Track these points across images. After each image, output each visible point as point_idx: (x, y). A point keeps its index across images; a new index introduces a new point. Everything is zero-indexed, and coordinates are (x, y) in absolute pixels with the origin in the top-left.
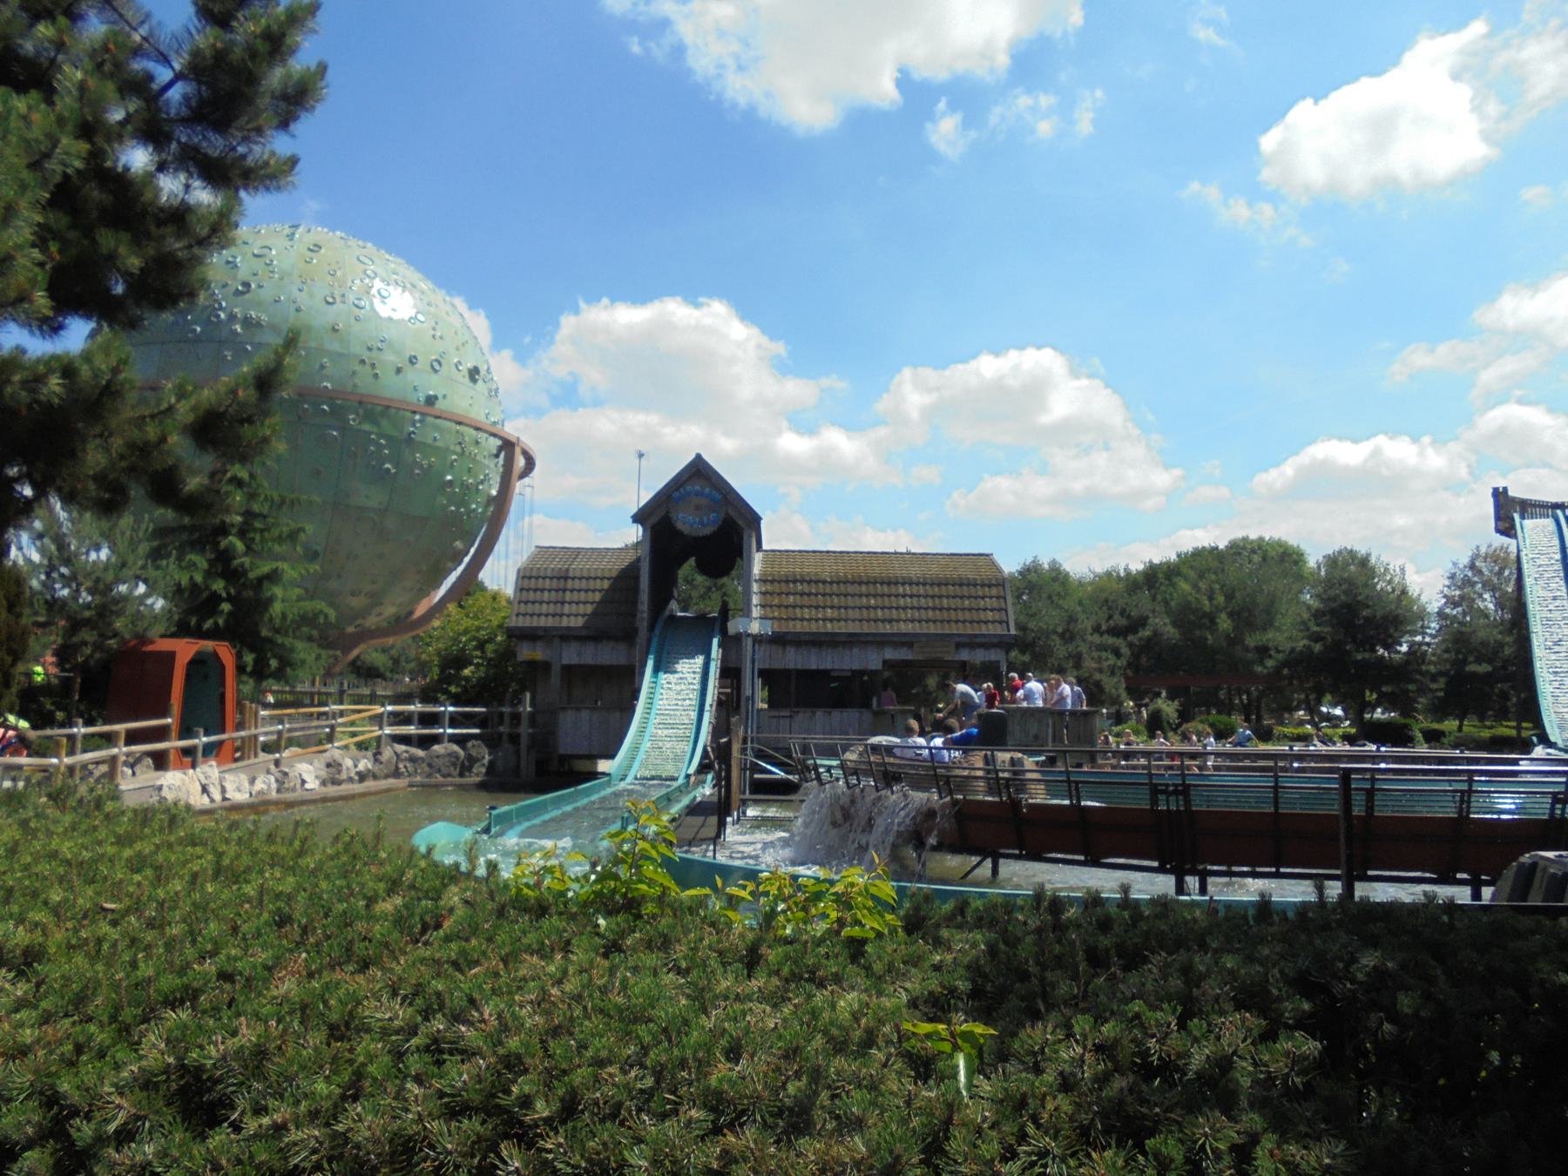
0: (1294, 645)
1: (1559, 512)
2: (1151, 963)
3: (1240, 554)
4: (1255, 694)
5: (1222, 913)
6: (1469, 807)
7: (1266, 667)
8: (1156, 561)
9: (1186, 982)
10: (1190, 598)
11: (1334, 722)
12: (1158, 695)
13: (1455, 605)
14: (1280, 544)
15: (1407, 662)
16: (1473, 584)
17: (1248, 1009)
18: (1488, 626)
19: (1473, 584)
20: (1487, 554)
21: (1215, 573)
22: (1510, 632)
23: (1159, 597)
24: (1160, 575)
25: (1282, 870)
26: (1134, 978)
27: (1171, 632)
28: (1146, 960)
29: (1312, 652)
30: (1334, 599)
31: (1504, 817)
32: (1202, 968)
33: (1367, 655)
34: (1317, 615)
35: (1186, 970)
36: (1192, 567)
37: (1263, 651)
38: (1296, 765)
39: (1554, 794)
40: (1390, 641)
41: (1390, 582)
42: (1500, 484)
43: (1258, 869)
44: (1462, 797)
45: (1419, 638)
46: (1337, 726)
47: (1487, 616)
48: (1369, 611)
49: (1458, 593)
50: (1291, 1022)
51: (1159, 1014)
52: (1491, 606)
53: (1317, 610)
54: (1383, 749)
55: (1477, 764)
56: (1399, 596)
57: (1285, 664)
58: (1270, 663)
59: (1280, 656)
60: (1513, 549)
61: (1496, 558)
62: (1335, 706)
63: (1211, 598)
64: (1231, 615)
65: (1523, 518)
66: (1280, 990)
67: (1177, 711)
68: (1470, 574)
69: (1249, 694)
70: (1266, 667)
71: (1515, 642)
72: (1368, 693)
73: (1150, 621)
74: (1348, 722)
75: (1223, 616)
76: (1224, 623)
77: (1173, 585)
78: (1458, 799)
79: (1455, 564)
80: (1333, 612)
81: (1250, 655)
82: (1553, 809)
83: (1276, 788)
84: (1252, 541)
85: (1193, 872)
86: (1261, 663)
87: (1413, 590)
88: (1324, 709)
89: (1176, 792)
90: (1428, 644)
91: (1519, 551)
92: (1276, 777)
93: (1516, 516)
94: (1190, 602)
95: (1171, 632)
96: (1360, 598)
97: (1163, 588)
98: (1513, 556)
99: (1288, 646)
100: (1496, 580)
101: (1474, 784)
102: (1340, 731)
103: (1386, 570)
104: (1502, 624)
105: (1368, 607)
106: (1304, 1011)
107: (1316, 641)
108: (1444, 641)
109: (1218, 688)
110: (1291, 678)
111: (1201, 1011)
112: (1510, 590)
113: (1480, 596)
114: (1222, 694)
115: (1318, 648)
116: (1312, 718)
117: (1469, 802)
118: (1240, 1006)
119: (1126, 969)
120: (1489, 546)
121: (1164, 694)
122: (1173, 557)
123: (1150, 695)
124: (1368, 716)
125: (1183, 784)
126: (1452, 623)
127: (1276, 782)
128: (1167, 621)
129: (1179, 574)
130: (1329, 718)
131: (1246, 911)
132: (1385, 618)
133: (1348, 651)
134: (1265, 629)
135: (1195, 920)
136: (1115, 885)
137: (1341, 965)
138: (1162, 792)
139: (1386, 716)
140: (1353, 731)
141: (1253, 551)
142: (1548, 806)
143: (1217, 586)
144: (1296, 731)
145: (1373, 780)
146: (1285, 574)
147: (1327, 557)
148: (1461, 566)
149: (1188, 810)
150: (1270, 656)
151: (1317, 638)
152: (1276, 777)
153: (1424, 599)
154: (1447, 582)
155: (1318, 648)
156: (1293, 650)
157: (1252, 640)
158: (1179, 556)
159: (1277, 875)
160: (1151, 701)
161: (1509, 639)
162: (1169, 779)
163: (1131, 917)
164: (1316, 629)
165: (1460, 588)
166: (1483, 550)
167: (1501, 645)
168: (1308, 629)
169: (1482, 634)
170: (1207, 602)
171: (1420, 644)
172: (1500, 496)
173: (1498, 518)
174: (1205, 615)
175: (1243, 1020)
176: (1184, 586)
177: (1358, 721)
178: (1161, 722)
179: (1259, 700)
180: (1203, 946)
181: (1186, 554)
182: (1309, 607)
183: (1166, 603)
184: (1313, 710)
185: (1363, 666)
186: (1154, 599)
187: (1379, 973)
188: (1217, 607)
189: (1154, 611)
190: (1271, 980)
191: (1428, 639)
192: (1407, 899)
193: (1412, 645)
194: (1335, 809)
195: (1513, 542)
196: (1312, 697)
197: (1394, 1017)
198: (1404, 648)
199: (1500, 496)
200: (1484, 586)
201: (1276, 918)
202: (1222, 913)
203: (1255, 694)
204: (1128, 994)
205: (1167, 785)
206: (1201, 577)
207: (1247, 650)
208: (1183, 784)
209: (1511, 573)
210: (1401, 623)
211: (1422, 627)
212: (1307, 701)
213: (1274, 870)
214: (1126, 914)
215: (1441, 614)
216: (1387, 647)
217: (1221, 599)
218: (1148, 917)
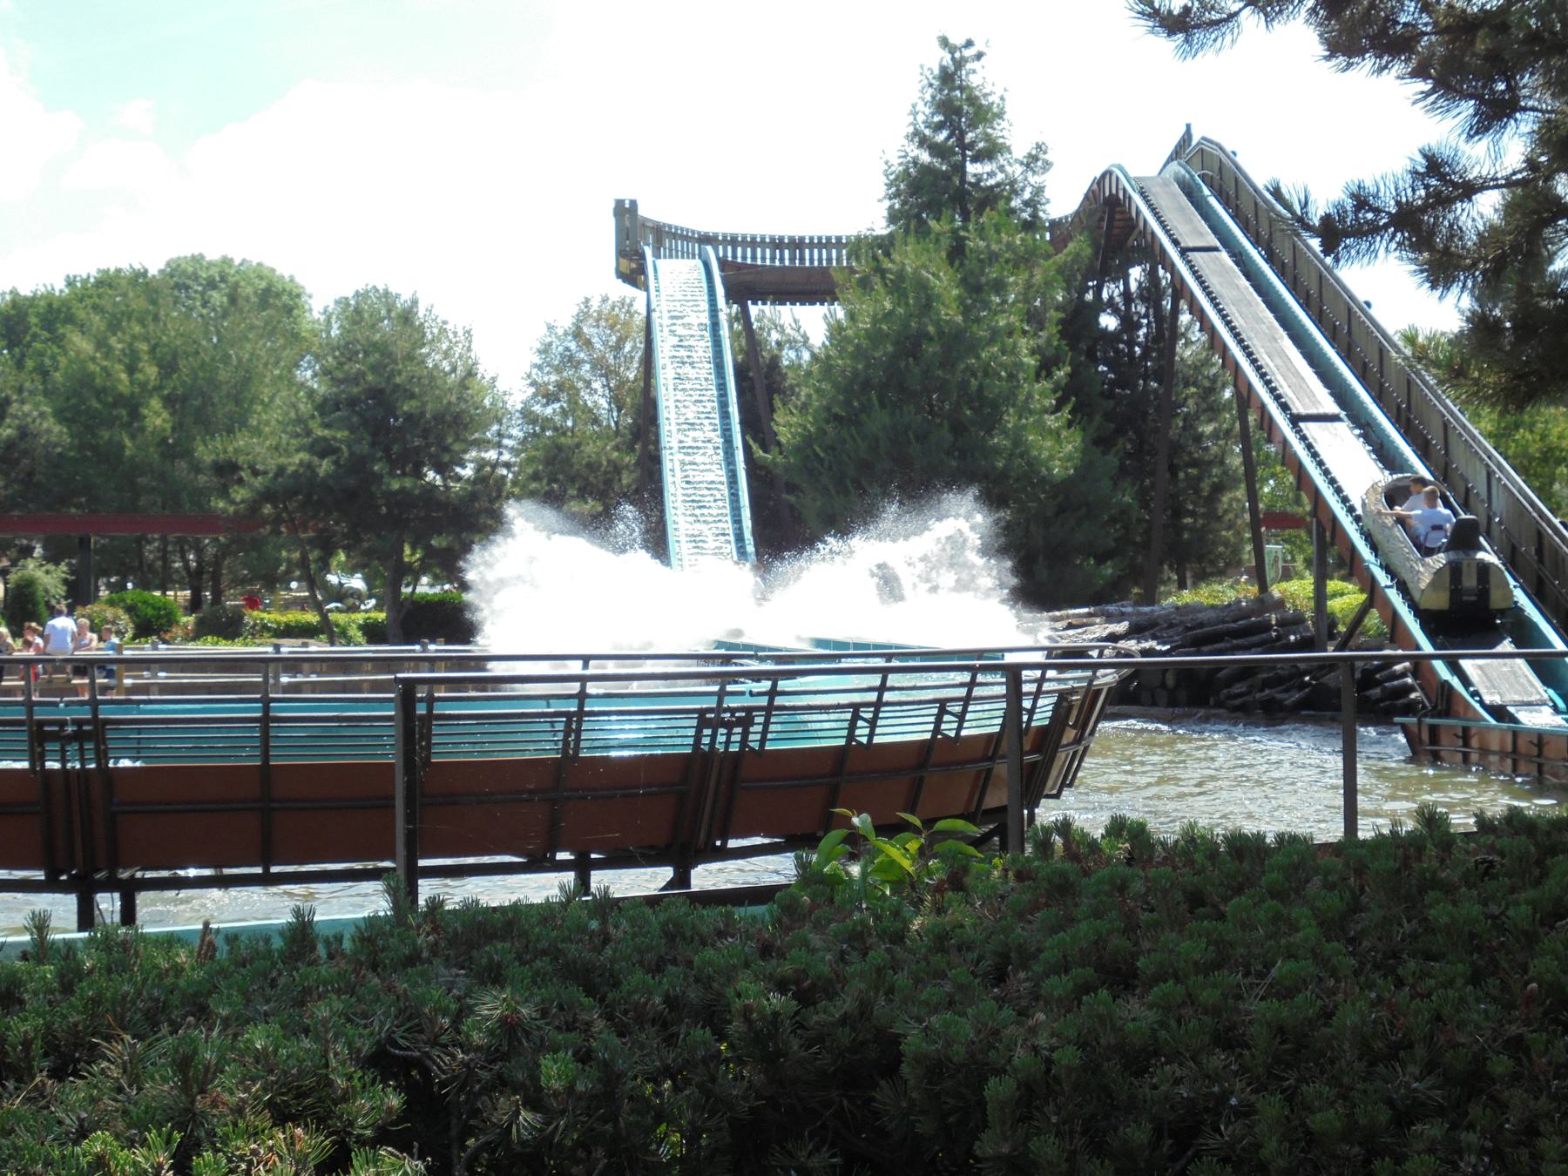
0: (283, 460)
1: (709, 249)
2: (105, 1057)
3: (187, 288)
4: (211, 550)
5: (223, 952)
6: (578, 740)
7: (233, 502)
8: (25, 291)
9: (185, 1088)
10: (92, 367)
11: (350, 601)
12: (27, 552)
13: (550, 398)
14: (260, 272)
15: (473, 496)
16: (577, 365)
17: (296, 1119)
18: (599, 436)
19: (577, 365)
20: (599, 313)
21: (141, 322)
22: (631, 449)
23: (30, 364)
24: (33, 320)
25: (275, 869)
26: (76, 1091)
27: (53, 431)
28: (94, 1054)
29: (315, 474)
30: (357, 379)
31: (614, 754)
32: (209, 1056)
33: (408, 483)
34: (325, 407)
35: (183, 1063)
36: (95, 307)
37: (227, 471)
38: (285, 679)
39: (702, 713)
40: (446, 458)
41: (447, 355)
42: (627, 196)
43: (227, 871)
44: (568, 724)
45: (491, 455)
46: (354, 609)
47: (596, 421)
48: (414, 403)
49: (553, 378)
50: (368, 1132)
51: (139, 1155)
52: (603, 402)
53: (325, 400)
54: (432, 647)
55: (793, 663)
56: (463, 379)
57: (268, 496)
58: (240, 494)
59: (258, 482)
60: (640, 307)
61: (613, 319)
62: (351, 570)
63: (131, 370)
64: (169, 401)
65: (657, 255)
66: (350, 1078)
67: (65, 582)
68: (573, 346)
69: (199, 551)
70: (233, 502)
71: (637, 463)
72: (407, 551)
73: (14, 408)
74: (373, 602)
75: (156, 403)
76: (157, 417)
77: (58, 340)
78: (560, 727)
79: (550, 328)
80: (353, 402)
81: (202, 479)
82: (698, 737)
83: (266, 720)
84: (211, 264)
85: (110, 885)
86: (224, 493)
87: (486, 370)
88: (333, 579)
89: (79, 737)
90: (507, 465)
91: (649, 311)
92: (266, 701)
93: (648, 251)
94: (92, 376)
95: (53, 431)
96: (398, 380)
97: (37, 345)
98: (639, 320)
99: (272, 463)
100: (611, 361)
101: (436, 704)
102: (359, 618)
103: (443, 331)
104: (617, 433)
105: (412, 396)
106: (390, 1109)
107: (322, 455)
108: (530, 460)
109: (140, 541)
110: (276, 521)
111: (212, 1134)
112: (632, 376)
113: (588, 384)
114: (150, 551)
115: (325, 467)
116: (313, 596)
117: (578, 732)
118: (282, 1117)
119: (58, 1074)
120: (605, 300)
121: (38, 551)
122: (60, 286)
123: (13, 553)
124: (406, 590)
125: (95, 720)
126: (543, 429)
127: (266, 709)
128: (48, 410)
129: (70, 319)
130: (340, 594)
131: (267, 940)
132: (439, 418)
133: (374, 474)
134: (230, 431)
135: (178, 970)
136: (21, 919)
137: (446, 1022)
138: (54, 737)
139: (437, 589)
140: (382, 616)
141: (212, 284)
142: (692, 732)
143: (144, 347)
144: (284, 619)
145: (582, 696)
146: (271, 331)
147: (343, 302)
148: (560, 332)
149: (103, 769)
150: (240, 481)
151: (323, 449)
152: (266, 701)
153: (501, 386)
154: (537, 360)
155: (325, 467)
156: (281, 470)
157: (207, 451)
158: (70, 283)
159: (267, 880)
160: (14, 563)
161: (629, 459)
162: (67, 710)
163: (61, 975)
164: (320, 432)
165: (558, 370)
166: (595, 304)
167: (617, 469)
168: (308, 433)
169: (590, 449)
170: (123, 376)
171: (495, 465)
172: (625, 213)
173: (621, 253)
174: (120, 400)
175: (291, 1142)
176: (81, 344)
177: (391, 599)
178: (35, 604)
179: (217, 562)
180: (202, 1013)
181: (85, 281)
182: (311, 393)
183: (44, 373)
184: (313, 581)
185: (402, 500)
186: (20, 365)
187: (510, 1028)
188: (143, 385)
189: (20, 390)
190: (333, 1063)
191: (506, 457)
192: (537, 899)
193: (481, 464)
194: (389, 753)
195: (640, 295)
196: (314, 555)
197: (535, 1101)
198: (467, 472)
199: (625, 213)
200: (594, 368)
201: (321, 951)
202: (223, 952)
203: (211, 550)
204: (70, 1122)
205: (63, 724)
206: (114, 326)
207: (197, 468)
208: (95, 720)
209: (634, 348)
210: (466, 427)
211: (500, 434)
212: (304, 563)
213: (258, 870)
214: (49, 971)
215: (527, 415)
216: (441, 469)
217: (151, 372)
218: (91, 971)
